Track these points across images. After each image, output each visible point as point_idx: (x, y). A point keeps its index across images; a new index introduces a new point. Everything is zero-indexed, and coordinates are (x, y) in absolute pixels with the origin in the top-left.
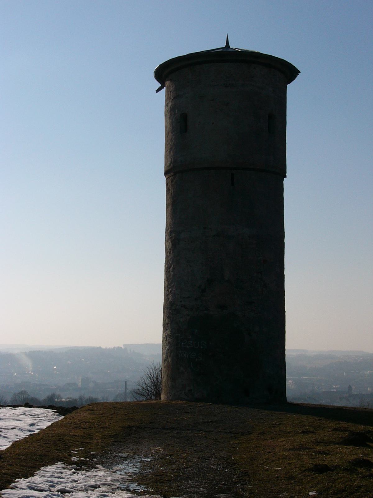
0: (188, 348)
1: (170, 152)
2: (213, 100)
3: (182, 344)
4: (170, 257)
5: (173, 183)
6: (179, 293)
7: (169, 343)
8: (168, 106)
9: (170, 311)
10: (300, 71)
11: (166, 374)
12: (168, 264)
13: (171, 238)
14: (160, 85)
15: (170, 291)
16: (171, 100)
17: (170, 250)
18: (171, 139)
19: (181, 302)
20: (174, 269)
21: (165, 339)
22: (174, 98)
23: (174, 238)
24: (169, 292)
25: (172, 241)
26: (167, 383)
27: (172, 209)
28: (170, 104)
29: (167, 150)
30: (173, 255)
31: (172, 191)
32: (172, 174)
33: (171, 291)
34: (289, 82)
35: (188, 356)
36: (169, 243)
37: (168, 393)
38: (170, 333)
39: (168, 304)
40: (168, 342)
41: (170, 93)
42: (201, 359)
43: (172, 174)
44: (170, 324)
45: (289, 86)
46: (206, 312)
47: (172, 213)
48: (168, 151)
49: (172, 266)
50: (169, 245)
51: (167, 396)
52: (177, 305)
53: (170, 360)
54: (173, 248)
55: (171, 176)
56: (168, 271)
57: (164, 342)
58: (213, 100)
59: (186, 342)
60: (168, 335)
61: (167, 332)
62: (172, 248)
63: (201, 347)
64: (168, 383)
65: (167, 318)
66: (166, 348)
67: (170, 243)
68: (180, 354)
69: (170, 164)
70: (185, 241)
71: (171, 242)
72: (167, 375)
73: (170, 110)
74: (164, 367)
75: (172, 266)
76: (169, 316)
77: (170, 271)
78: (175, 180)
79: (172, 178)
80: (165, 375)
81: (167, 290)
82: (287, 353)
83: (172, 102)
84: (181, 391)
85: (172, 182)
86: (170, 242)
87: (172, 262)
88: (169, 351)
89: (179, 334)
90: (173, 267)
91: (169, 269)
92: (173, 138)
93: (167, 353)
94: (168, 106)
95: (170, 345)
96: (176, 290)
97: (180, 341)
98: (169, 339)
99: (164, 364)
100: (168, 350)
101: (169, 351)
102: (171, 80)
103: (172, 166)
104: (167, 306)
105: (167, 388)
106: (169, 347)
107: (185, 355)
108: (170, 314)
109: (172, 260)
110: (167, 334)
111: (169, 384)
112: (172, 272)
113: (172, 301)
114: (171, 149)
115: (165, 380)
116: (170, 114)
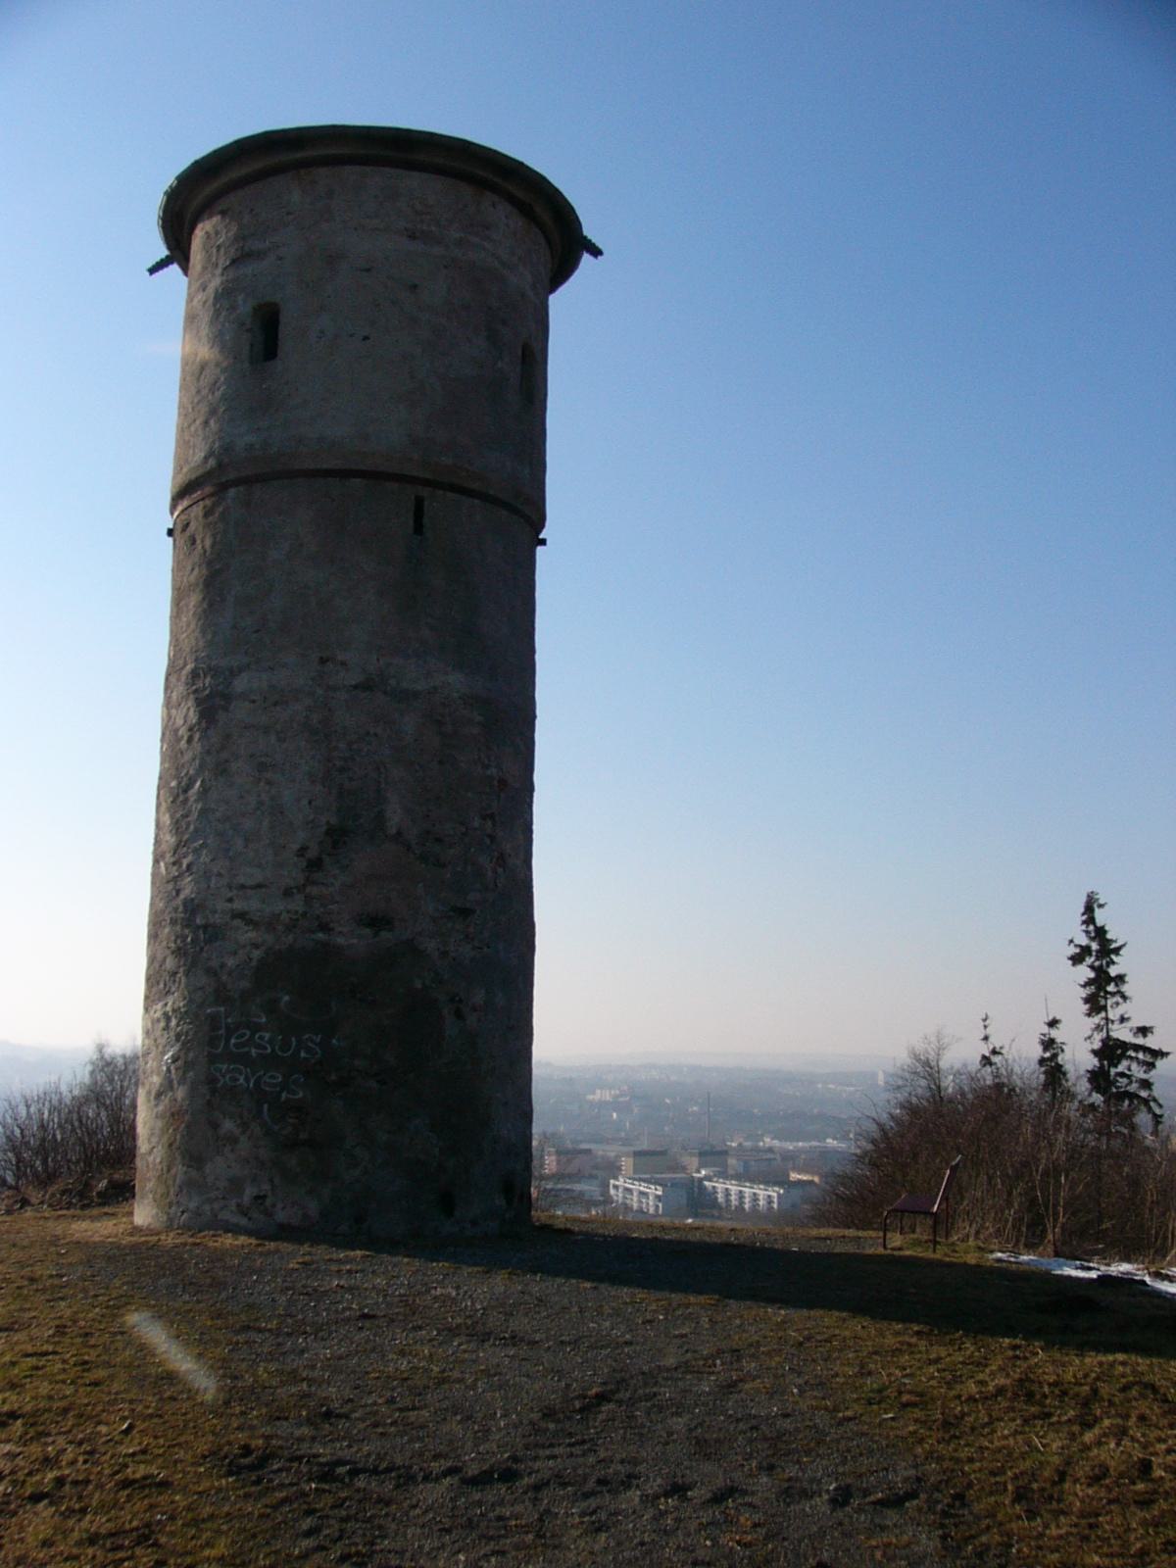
0: (254, 1055)
1: (206, 423)
2: (368, 270)
3: (233, 1041)
4: (188, 756)
5: (211, 518)
6: (222, 871)
7: (178, 1037)
8: (204, 290)
9: (187, 931)
10: (600, 246)
11: (165, 1139)
12: (177, 777)
13: (196, 691)
14: (163, 252)
15: (184, 866)
16: (219, 271)
17: (190, 729)
18: (216, 382)
19: (230, 900)
20: (205, 791)
21: (162, 1024)
22: (233, 262)
23: (207, 692)
24: (181, 866)
25: (199, 702)
26: (169, 1171)
27: (204, 599)
28: (216, 283)
29: (195, 421)
30: (203, 746)
31: (208, 543)
32: (208, 489)
33: (189, 866)
34: (553, 288)
35: (252, 1081)
36: (189, 709)
37: (170, 1205)
38: (181, 1004)
39: (176, 910)
40: (172, 1034)
41: (218, 251)
42: (301, 1095)
43: (208, 489)
44: (187, 974)
45: (552, 298)
46: (320, 935)
47: (204, 611)
48: (198, 422)
49: (198, 784)
50: (186, 717)
51: (168, 1214)
52: (215, 912)
53: (181, 1093)
54: (204, 725)
55: (203, 499)
56: (181, 798)
57: (158, 1033)
58: (368, 270)
59: (266, 1048)
60: (174, 1011)
61: (170, 1000)
62: (199, 723)
63: (303, 1054)
64: (173, 1171)
65: (173, 953)
66: (163, 1053)
67: (192, 710)
68: (224, 1076)
69: (206, 458)
70: (254, 702)
71: (198, 706)
72: (170, 1145)
73: (215, 298)
74: (157, 1117)
75: (198, 784)
76: (179, 949)
77: (186, 800)
78: (221, 509)
79: (208, 502)
80: (158, 1143)
81: (174, 864)
82: (535, 1071)
83: (222, 274)
84: (223, 1198)
85: (206, 515)
86: (190, 704)
87: (202, 767)
88: (179, 1063)
89: (222, 1009)
90: (201, 786)
91: (185, 791)
92: (222, 379)
93: (169, 1070)
94: (204, 290)
95: (183, 1044)
96: (212, 860)
97: (222, 1032)
98: (178, 1025)
99: (156, 1105)
100: (173, 1062)
101: (180, 1063)
102: (223, 213)
103: (212, 462)
104: (174, 915)
105: (168, 1187)
106: (180, 1050)
107: (242, 1080)
108: (184, 941)
109: (197, 762)
110: (169, 1008)
111: (176, 1175)
112: (196, 801)
113: (192, 900)
114: (213, 412)
115: (158, 1160)
116: (215, 310)
